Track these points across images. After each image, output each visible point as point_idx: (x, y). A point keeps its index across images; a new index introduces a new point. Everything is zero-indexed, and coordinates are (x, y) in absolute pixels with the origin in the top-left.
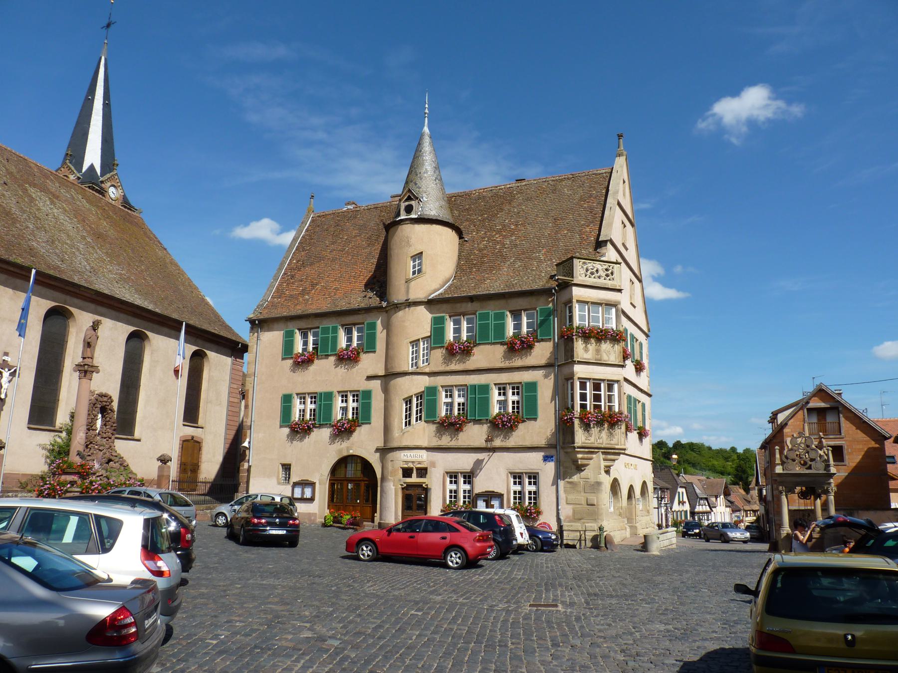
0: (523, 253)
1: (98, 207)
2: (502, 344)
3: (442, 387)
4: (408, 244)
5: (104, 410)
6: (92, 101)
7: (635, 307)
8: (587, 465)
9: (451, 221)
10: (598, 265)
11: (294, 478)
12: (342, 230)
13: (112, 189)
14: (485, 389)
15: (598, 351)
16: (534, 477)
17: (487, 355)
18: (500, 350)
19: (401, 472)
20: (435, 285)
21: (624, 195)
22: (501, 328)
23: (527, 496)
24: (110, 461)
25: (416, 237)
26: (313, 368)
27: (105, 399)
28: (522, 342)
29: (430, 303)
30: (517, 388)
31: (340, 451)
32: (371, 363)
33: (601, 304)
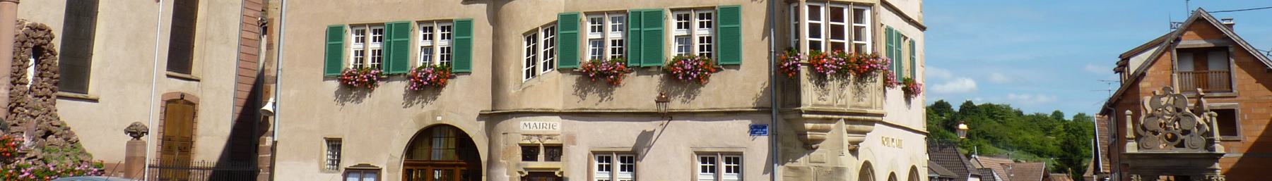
5: (38, 52)
8: (820, 140)
11: (347, 162)
19: (519, 151)
24: (48, 133)
27: (41, 34)
31: (421, 118)
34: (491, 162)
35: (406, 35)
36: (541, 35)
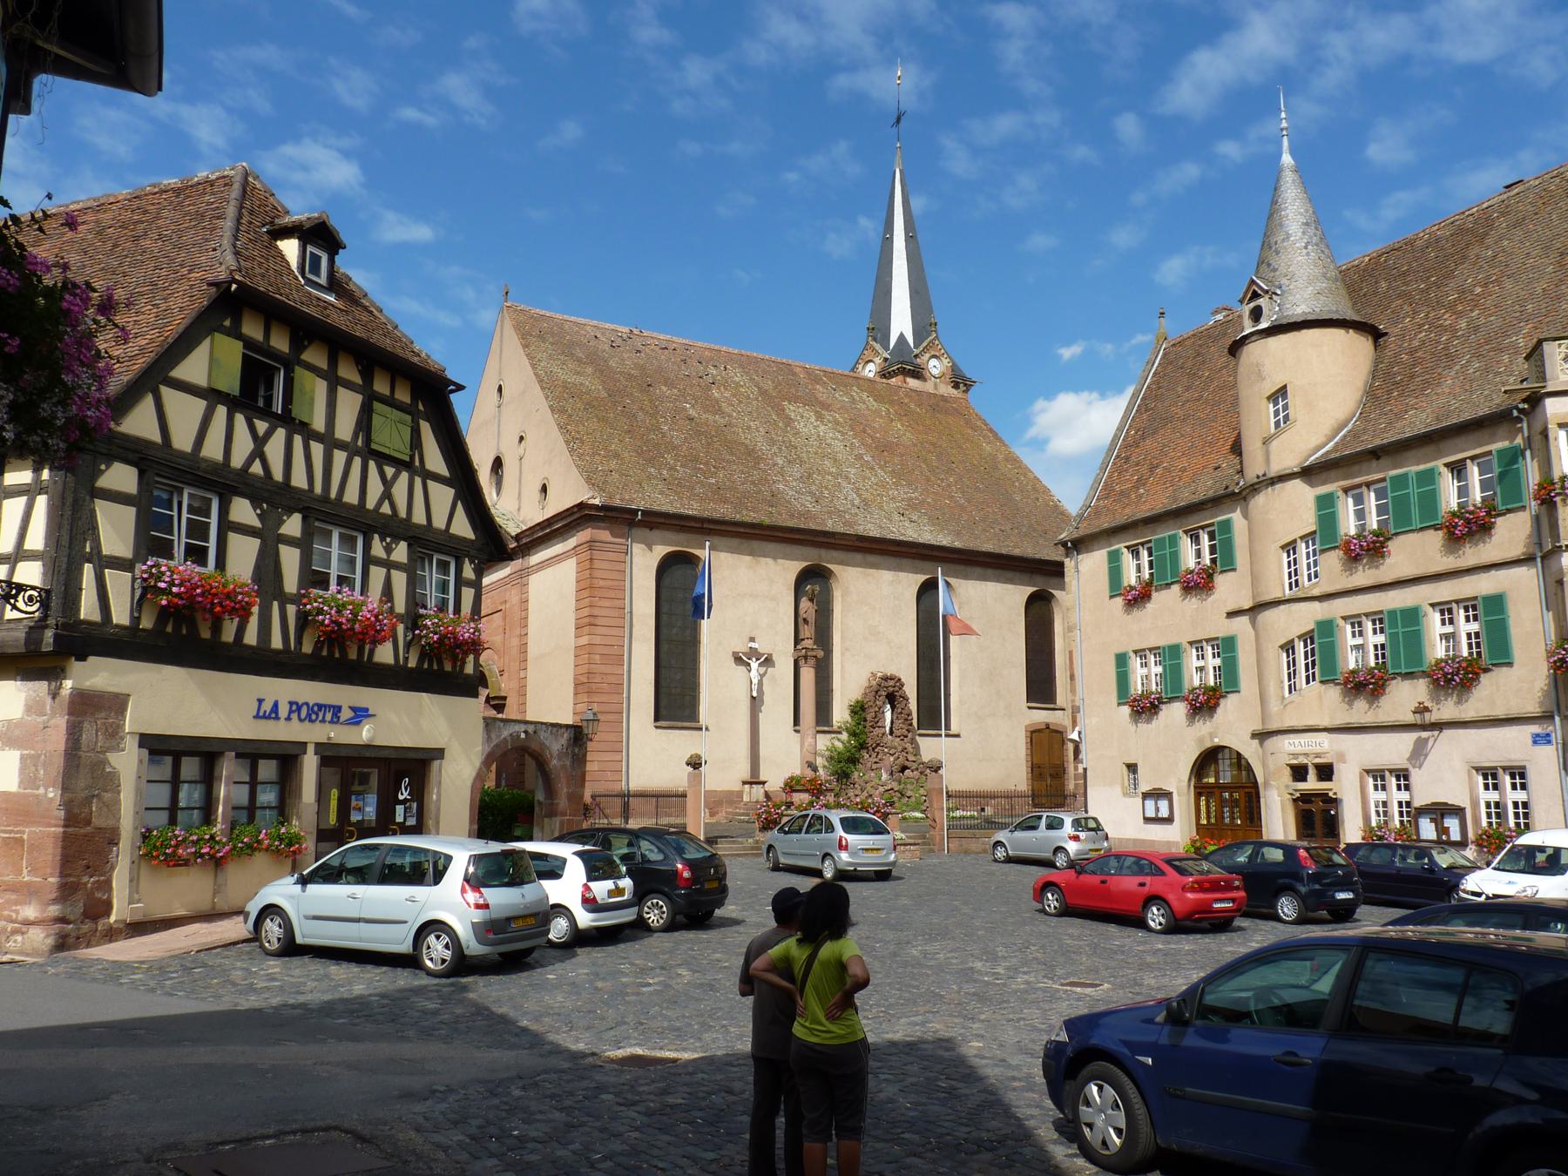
1: (892, 402)
2: (1436, 528)
3: (1344, 618)
4: (1261, 377)
5: (892, 699)
6: (891, 240)
9: (1351, 315)
13: (933, 362)
14: (1412, 616)
16: (1519, 775)
17: (1415, 551)
18: (1436, 538)
19: (1288, 771)
20: (1315, 441)
22: (1430, 500)
23: (1396, 809)
24: (903, 769)
25: (1273, 359)
26: (1150, 606)
27: (891, 683)
28: (1468, 521)
29: (1308, 473)
30: (1471, 605)
31: (1201, 740)
32: (1231, 590)
34: (1266, 783)
35: (1331, 634)
36: (1300, 648)
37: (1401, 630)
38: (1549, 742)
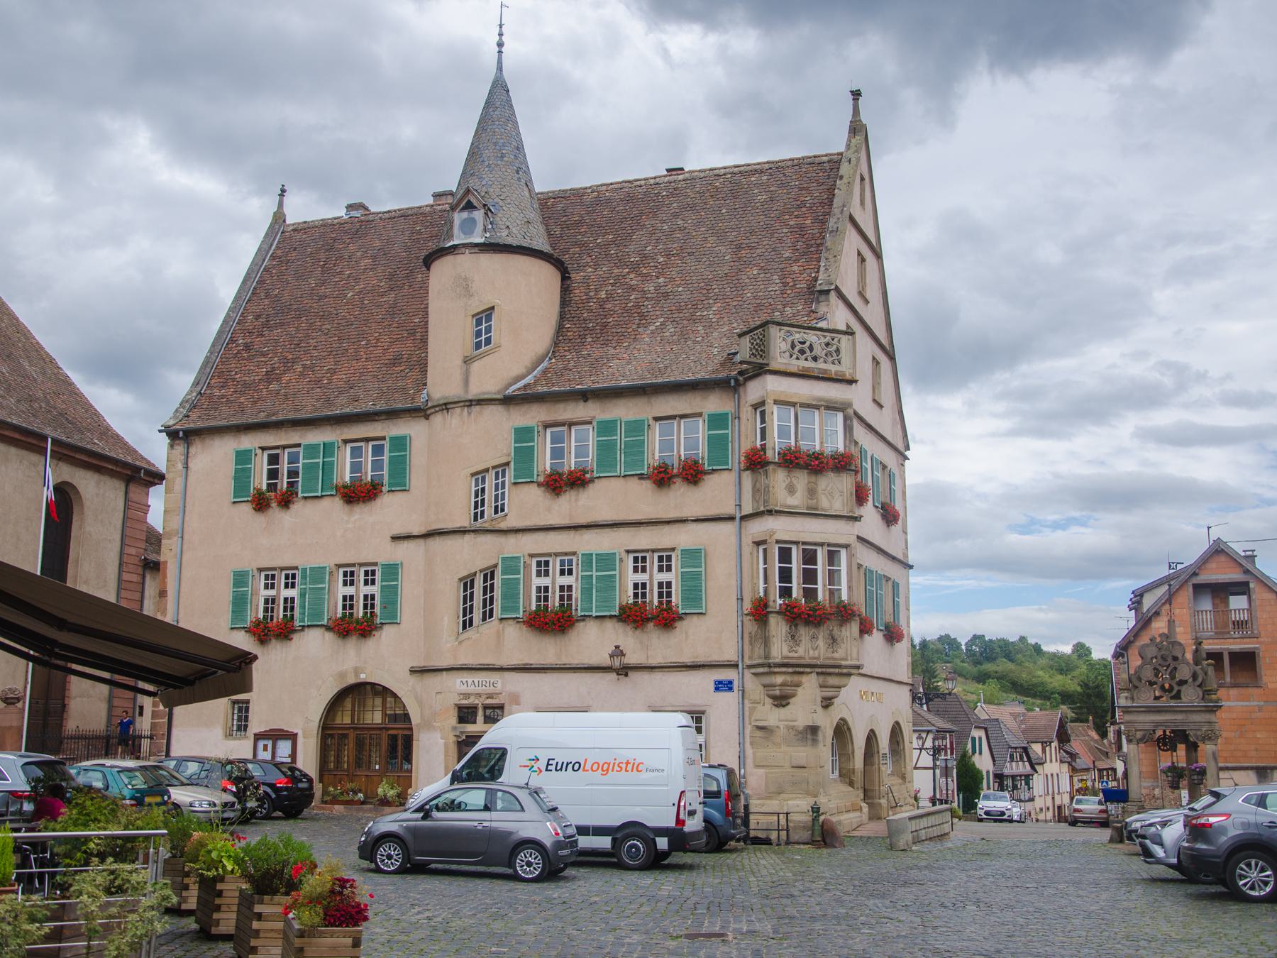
0: (679, 310)
7: (881, 406)
8: (793, 696)
9: (546, 248)
10: (812, 337)
11: (255, 726)
12: (341, 258)
15: (812, 492)
20: (518, 369)
21: (862, 203)
33: (817, 407)
37: (595, 574)
38: (731, 689)
